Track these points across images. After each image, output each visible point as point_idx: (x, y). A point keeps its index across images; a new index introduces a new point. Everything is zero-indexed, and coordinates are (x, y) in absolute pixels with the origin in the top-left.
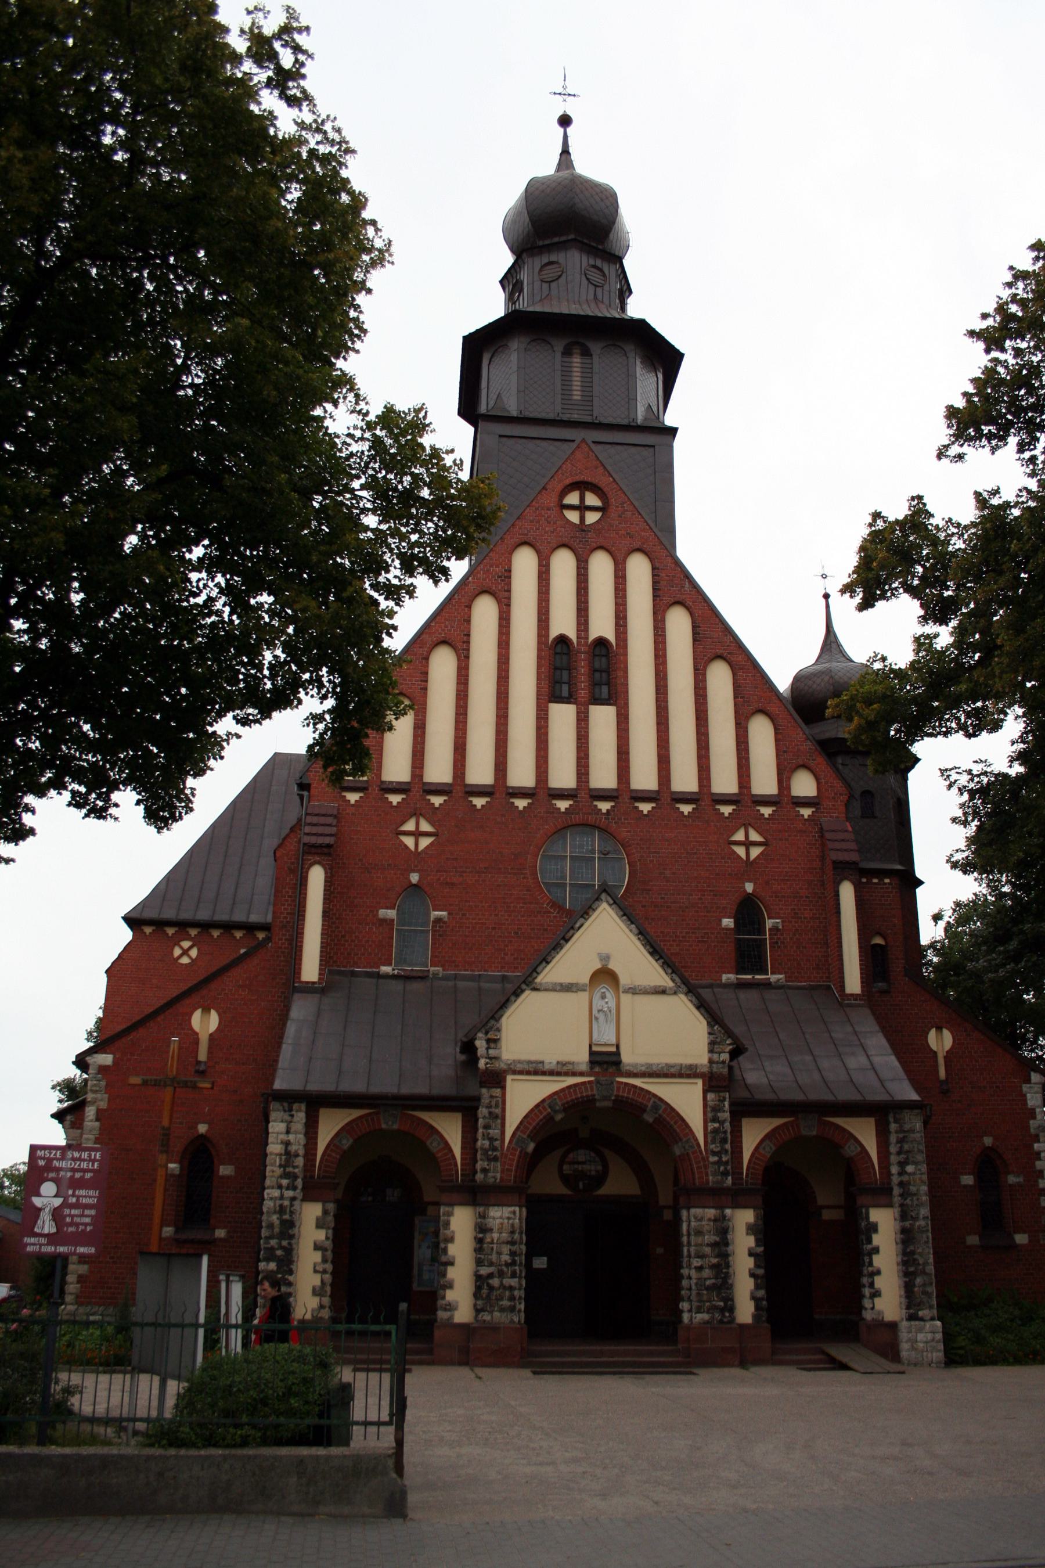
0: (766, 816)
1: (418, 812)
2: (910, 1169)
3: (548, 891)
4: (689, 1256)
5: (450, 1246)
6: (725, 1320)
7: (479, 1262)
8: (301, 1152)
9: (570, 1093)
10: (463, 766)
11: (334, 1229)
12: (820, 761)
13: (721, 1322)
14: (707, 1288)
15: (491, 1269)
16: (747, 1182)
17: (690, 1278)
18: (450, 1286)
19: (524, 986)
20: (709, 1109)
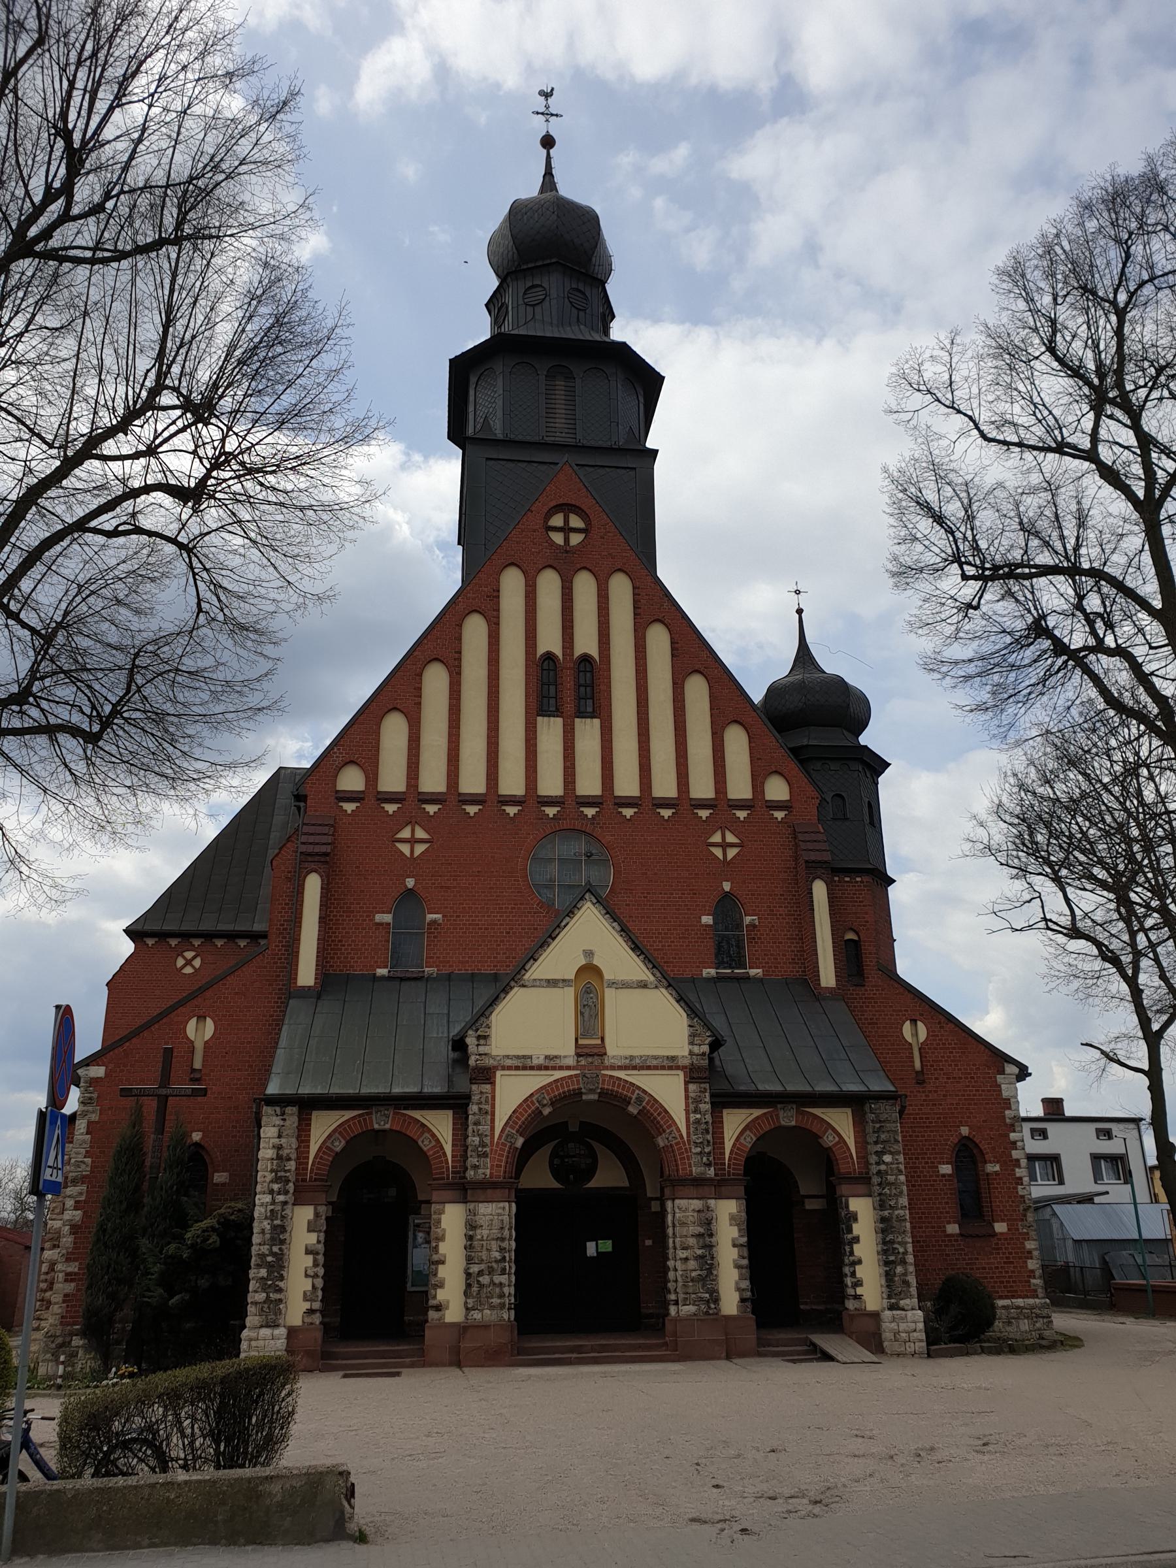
1: (413, 821)
2: (887, 1158)
4: (675, 1248)
5: (441, 1245)
6: (711, 1312)
7: (469, 1260)
8: (293, 1156)
9: (557, 1087)
10: (457, 776)
11: (326, 1232)
12: (793, 766)
13: (707, 1313)
14: (692, 1280)
15: (483, 1266)
16: (729, 1172)
17: (676, 1270)
18: (441, 1285)
19: (512, 984)
20: (690, 1101)
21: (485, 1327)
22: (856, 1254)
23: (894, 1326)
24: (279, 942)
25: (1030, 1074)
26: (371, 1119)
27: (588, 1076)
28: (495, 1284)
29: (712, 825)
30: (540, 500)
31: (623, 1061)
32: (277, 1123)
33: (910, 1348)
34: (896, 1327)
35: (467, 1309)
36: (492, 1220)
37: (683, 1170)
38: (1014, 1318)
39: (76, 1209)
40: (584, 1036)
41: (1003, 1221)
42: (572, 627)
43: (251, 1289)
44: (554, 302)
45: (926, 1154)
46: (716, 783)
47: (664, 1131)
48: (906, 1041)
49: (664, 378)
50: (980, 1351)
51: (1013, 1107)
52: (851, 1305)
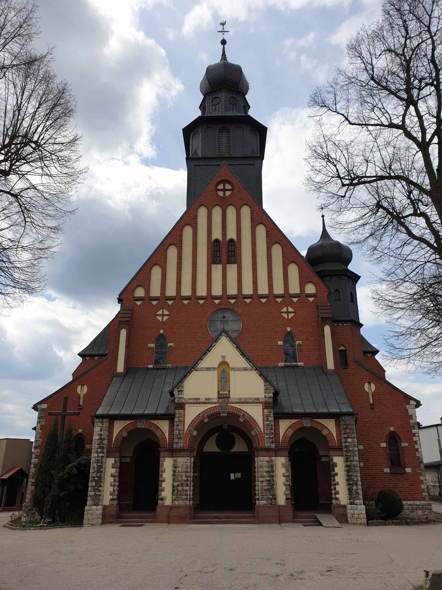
0: (295, 301)
2: (349, 440)
3: (212, 334)
5: (164, 474)
6: (273, 503)
7: (174, 480)
9: (210, 411)
12: (317, 279)
13: (271, 504)
14: (265, 490)
15: (179, 483)
16: (282, 446)
18: (163, 490)
20: (265, 416)
21: (179, 507)
22: (336, 480)
23: (352, 511)
24: (112, 356)
25: (421, 405)
26: (137, 424)
27: (223, 406)
28: (184, 490)
29: (283, 304)
30: (214, 179)
31: (237, 400)
32: (100, 425)
33: (359, 521)
34: (353, 512)
35: (173, 500)
36: (183, 464)
37: (261, 444)
38: (415, 509)
39: (36, 458)
40: (222, 390)
41: (409, 467)
42: (226, 228)
43: (89, 490)
44: (223, 103)
45: (375, 438)
46: (285, 287)
47: (254, 429)
48: (366, 391)
49: (267, 128)
50: (391, 523)
51: (414, 419)
52: (334, 502)
